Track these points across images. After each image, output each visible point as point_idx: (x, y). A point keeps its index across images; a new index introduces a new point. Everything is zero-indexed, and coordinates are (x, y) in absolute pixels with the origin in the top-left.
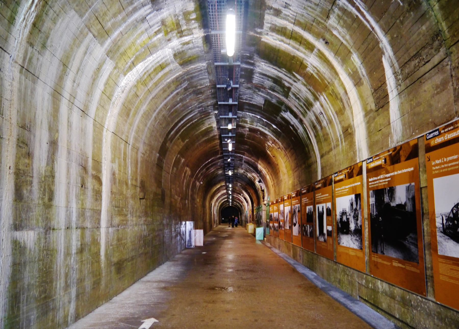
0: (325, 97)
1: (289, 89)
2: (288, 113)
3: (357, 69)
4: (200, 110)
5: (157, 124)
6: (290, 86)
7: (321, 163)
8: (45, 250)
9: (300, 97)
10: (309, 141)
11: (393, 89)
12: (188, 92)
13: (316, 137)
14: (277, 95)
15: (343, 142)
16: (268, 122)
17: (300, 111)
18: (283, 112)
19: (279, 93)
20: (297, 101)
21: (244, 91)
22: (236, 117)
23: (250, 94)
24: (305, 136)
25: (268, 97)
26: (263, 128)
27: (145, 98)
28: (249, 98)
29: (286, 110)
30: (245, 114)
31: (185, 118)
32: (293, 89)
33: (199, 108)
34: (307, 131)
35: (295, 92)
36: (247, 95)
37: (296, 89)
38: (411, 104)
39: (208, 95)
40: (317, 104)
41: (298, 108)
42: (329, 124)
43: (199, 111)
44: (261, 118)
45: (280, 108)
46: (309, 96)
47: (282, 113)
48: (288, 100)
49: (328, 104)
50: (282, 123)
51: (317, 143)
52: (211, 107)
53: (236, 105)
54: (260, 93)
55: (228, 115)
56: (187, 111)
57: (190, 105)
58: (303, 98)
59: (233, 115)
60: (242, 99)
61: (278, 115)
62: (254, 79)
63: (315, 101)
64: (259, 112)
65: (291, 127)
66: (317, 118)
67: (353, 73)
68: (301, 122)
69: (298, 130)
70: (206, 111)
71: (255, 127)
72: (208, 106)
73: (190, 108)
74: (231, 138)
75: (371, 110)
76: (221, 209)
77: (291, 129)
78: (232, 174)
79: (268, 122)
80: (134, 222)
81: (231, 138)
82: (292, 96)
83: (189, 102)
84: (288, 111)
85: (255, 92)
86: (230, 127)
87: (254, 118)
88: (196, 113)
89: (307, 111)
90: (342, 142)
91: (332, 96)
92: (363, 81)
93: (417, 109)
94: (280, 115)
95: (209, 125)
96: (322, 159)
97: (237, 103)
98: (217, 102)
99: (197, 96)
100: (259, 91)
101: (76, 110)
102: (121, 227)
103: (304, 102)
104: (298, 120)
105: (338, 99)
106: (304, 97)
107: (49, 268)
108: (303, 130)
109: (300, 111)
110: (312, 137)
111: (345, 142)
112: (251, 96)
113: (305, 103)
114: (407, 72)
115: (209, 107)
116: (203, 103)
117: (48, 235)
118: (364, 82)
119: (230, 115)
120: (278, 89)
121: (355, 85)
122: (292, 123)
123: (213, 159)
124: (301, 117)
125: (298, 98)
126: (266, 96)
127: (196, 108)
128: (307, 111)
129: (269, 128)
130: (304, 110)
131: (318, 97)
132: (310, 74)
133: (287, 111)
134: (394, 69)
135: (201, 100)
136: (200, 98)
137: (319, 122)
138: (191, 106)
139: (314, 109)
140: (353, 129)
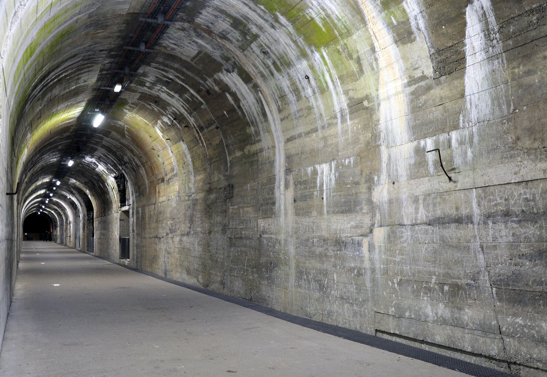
1: (256, 37)
3: (408, 20)
6: (260, 33)
11: (477, 51)
18: (225, 72)
32: (263, 38)
34: (262, 102)
37: (269, 38)
38: (513, 73)
47: (220, 74)
49: (326, 64)
58: (276, 53)
61: (211, 76)
62: (201, 16)
63: (298, 58)
67: (398, 24)
75: (424, 78)
76: (26, 216)
84: (236, 70)
89: (275, 72)
92: (415, 37)
93: (527, 80)
95: (85, 81)
100: (199, 36)
111: (351, 119)
114: (511, 30)
118: (418, 38)
120: (234, 35)
121: (396, 42)
122: (234, 89)
128: (275, 72)
131: (309, 52)
132: (309, 18)
133: (233, 71)
134: (487, 23)
139: (292, 72)
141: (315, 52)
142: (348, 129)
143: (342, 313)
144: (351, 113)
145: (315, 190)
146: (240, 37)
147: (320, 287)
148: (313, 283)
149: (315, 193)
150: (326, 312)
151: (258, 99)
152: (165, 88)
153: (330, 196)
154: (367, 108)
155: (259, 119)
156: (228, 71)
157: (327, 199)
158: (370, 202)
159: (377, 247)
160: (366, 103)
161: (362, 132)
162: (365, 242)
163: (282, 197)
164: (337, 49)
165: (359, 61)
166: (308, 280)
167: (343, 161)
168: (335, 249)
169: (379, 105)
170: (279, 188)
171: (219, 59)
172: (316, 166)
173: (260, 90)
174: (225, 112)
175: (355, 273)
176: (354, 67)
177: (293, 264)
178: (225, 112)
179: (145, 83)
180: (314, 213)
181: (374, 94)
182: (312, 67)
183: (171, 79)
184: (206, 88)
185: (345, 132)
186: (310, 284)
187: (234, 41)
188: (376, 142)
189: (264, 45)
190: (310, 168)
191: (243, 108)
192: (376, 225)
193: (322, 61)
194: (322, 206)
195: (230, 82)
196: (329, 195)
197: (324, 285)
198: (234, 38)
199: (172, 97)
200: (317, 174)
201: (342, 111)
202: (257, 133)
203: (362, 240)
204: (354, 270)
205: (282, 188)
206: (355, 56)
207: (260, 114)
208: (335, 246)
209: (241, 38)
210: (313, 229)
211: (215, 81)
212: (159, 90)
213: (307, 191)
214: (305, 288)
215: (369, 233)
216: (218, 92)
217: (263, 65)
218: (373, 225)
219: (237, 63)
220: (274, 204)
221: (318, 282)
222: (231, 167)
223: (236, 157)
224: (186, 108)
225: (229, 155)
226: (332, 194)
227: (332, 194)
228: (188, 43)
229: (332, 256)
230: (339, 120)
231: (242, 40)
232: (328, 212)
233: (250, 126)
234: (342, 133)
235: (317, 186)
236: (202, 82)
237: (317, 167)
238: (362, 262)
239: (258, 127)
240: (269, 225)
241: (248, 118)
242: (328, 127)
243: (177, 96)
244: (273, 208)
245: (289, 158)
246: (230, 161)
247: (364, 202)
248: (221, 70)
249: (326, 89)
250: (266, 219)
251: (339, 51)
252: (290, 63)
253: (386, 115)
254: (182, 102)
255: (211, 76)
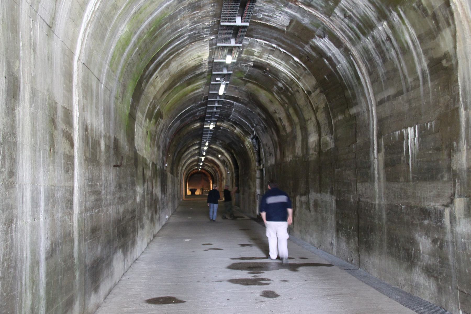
0: (402, 13)
2: (326, 40)
4: (191, 34)
5: (135, 54)
7: (377, 113)
8: (6, 260)
9: (352, 15)
10: (355, 81)
12: (183, 5)
13: (370, 74)
14: (313, 12)
15: (427, 81)
16: (287, 52)
17: (348, 36)
18: (318, 38)
19: (317, 9)
20: (346, 20)
21: (261, 5)
22: (241, 45)
23: (270, 11)
24: (349, 72)
25: (298, 15)
26: (276, 62)
27: (126, 11)
28: (266, 17)
29: (323, 36)
30: (254, 41)
31: (169, 46)
33: (191, 30)
34: (354, 65)
35: (346, 7)
36: (265, 12)
39: (208, 12)
40: (382, 25)
41: (344, 32)
42: (400, 55)
43: (189, 35)
44: (278, 48)
45: (314, 32)
46: (370, 14)
47: (314, 40)
48: (331, 20)
50: (312, 55)
51: (372, 83)
52: (207, 30)
53: (246, 27)
54: (287, 10)
55: (229, 42)
56: (175, 35)
57: (180, 26)
58: (358, 16)
59: (236, 43)
60: (255, 18)
63: (379, 20)
64: (276, 39)
65: (325, 60)
66: (378, 46)
68: (347, 52)
69: (337, 64)
70: (200, 35)
71: (264, 60)
72: (203, 28)
73: (179, 30)
74: (223, 76)
77: (324, 62)
78: (213, 128)
79: (287, 52)
80: (109, 202)
81: (223, 76)
82: (338, 13)
83: (181, 20)
84: (327, 36)
85: (278, 7)
86: (229, 60)
87: (266, 47)
88: (185, 38)
90: (425, 82)
91: (416, 12)
94: (310, 42)
96: (380, 106)
97: (247, 24)
98: (219, 22)
99: (193, 11)
101: (39, 23)
102: (95, 210)
103: (358, 21)
104: (342, 49)
105: (427, 15)
106: (359, 14)
107: (11, 291)
108: (348, 65)
109: (348, 36)
110: (363, 74)
111: (432, 80)
112: (271, 14)
113: (361, 24)
115: (205, 30)
116: (199, 23)
117: (9, 235)
119: (233, 43)
122: (329, 54)
123: (193, 106)
124: (348, 45)
125: (350, 17)
126: (294, 14)
127: (187, 31)
128: (361, 35)
129: (286, 62)
130: (356, 34)
133: (325, 37)
135: (196, 19)
136: (197, 15)
137: (382, 53)
138: (182, 27)
139: (375, 33)
140: (454, 62)
141: (393, 12)
142: (429, 92)
143: (428, 287)
144: (431, 73)
145: (402, 155)
146: (323, 3)
147: (408, 256)
148: (402, 252)
149: (402, 158)
150: (414, 283)
151: (350, 62)
152: (272, 56)
153: (415, 161)
154: (446, 69)
155: (354, 82)
156: (320, 37)
157: (412, 164)
158: (449, 169)
159: (155, 145)
160: (444, 62)
161: (442, 94)
162: (447, 212)
163: (376, 160)
164: (412, 7)
165: (434, 16)
166: (399, 248)
167: (425, 125)
168: (420, 217)
169: (457, 63)
170: (373, 152)
171: (311, 27)
172: (403, 130)
173: (351, 54)
174: (325, 77)
175: (439, 245)
176: (431, 24)
177: (386, 231)
178: (325, 77)
179: (254, 53)
180: (402, 179)
181: (451, 53)
182: (392, 27)
183: (274, 48)
184: (306, 54)
185: (426, 94)
186: (400, 252)
187: (319, 7)
188: (454, 104)
189: (346, 9)
190: (397, 132)
191: (339, 72)
192: (456, 195)
193: (400, 21)
194: (408, 171)
195: (324, 47)
196: (413, 161)
197: (411, 255)
198: (318, 5)
199: (280, 64)
200: (403, 139)
201: (423, 72)
202: (354, 96)
203: (443, 210)
204: (437, 241)
205: (375, 152)
206: (430, 12)
207: (354, 76)
208: (420, 214)
209: (324, 4)
210: (401, 196)
211: (311, 46)
212: (268, 58)
213: (395, 156)
214: (396, 255)
215: (449, 204)
216: (316, 57)
217: (349, 29)
218: (453, 195)
219: (326, 29)
220: (369, 167)
221: (406, 251)
222: (335, 130)
223: (339, 120)
224: (294, 74)
225: (334, 118)
226: (416, 160)
227: (416, 160)
228: (279, 13)
229: (417, 224)
230: (421, 83)
231: (326, 6)
232: (413, 178)
233: (347, 90)
234: (424, 96)
235: (403, 151)
236: (301, 49)
237: (404, 131)
238: (445, 233)
239: (354, 90)
240: (366, 189)
241: (344, 81)
242: (412, 90)
243: (283, 63)
244: (369, 172)
245: (380, 121)
246: (335, 124)
247: (445, 170)
248: (315, 36)
249: (408, 50)
250: (363, 183)
251: (414, 9)
252: (372, 25)
253: (464, 75)
254: (289, 68)
255: (307, 43)
